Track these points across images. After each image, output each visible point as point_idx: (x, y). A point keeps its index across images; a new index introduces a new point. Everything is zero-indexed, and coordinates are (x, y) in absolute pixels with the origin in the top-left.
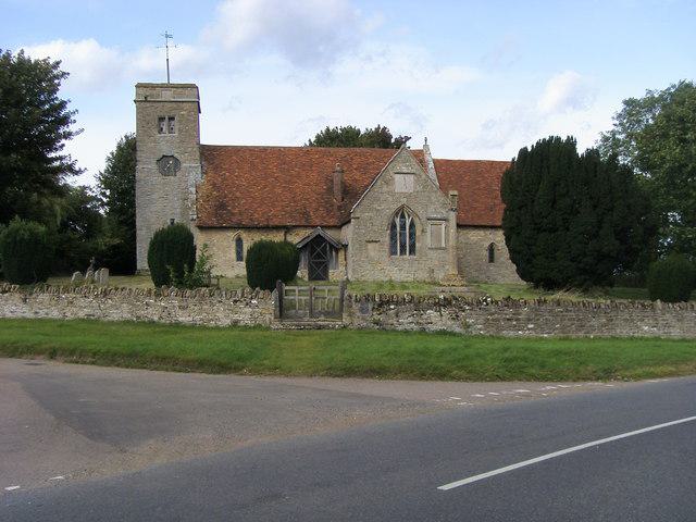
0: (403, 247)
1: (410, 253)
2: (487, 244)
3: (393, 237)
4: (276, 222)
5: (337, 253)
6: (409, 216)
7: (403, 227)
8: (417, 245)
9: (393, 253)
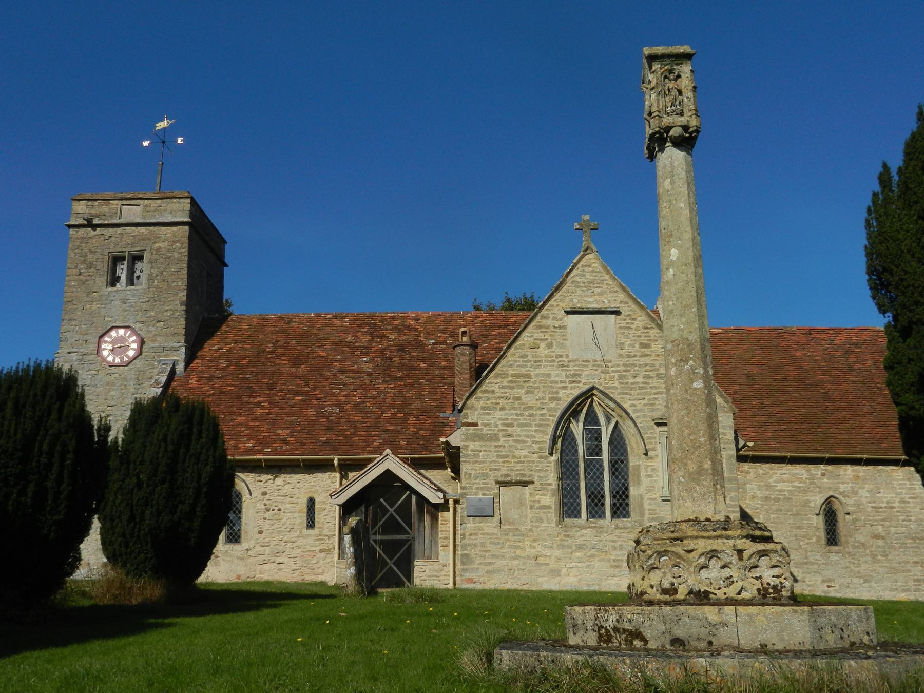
0: (595, 500)
1: (614, 514)
2: (818, 500)
3: (567, 469)
4: (513, 477)
5: (435, 519)
6: (608, 419)
7: (594, 449)
8: (633, 491)
9: (568, 508)
